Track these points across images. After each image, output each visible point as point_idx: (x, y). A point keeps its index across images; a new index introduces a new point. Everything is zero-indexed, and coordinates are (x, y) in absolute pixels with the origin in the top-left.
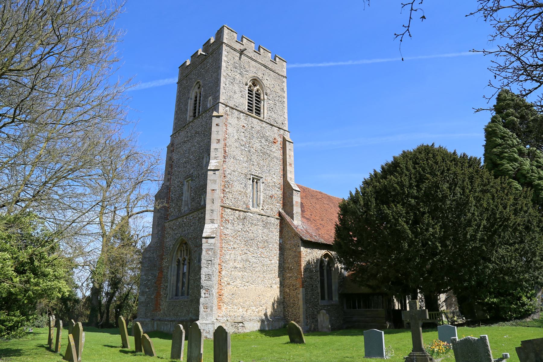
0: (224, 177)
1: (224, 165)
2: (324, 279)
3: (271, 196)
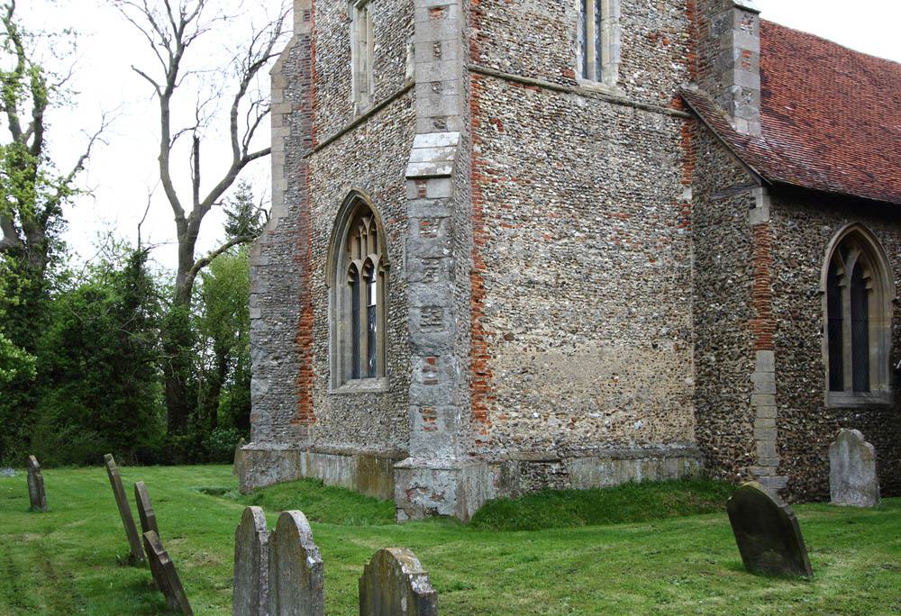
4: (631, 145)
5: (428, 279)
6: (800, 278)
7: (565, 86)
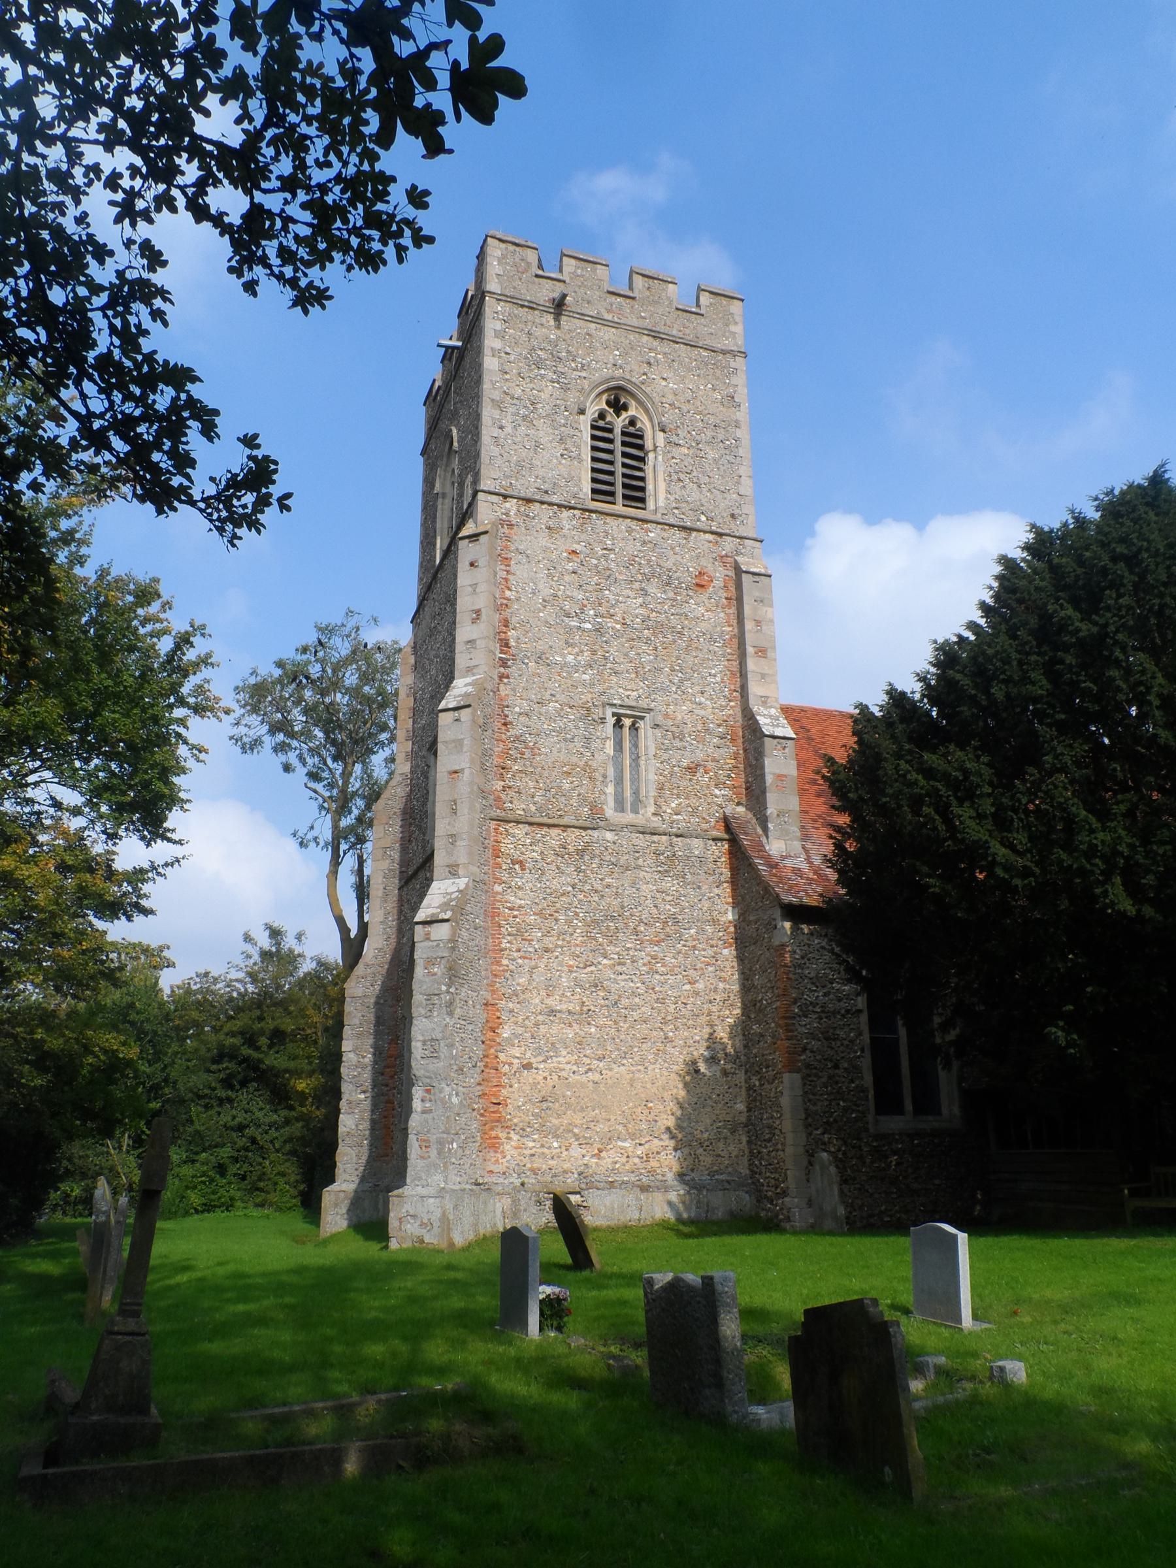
0: (505, 724)
1: (502, 687)
2: (897, 1039)
3: (692, 765)
4: (666, 871)
5: (429, 1014)
6: (831, 996)
7: (595, 821)
